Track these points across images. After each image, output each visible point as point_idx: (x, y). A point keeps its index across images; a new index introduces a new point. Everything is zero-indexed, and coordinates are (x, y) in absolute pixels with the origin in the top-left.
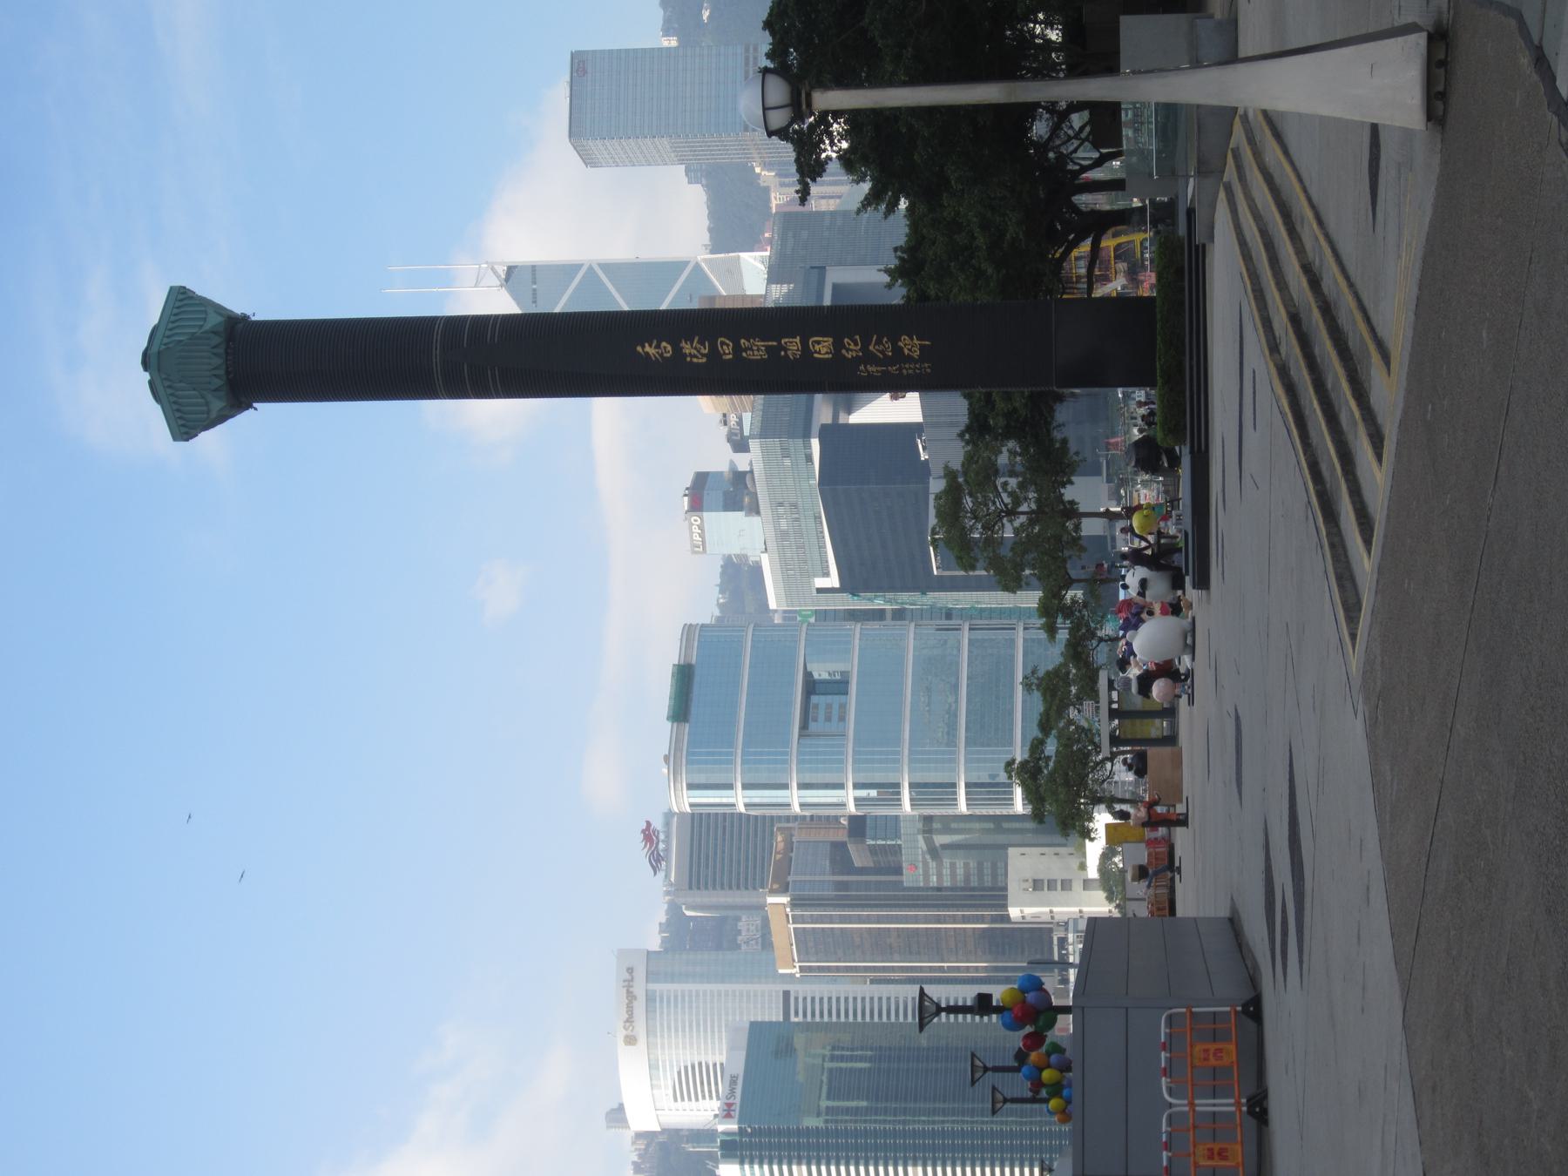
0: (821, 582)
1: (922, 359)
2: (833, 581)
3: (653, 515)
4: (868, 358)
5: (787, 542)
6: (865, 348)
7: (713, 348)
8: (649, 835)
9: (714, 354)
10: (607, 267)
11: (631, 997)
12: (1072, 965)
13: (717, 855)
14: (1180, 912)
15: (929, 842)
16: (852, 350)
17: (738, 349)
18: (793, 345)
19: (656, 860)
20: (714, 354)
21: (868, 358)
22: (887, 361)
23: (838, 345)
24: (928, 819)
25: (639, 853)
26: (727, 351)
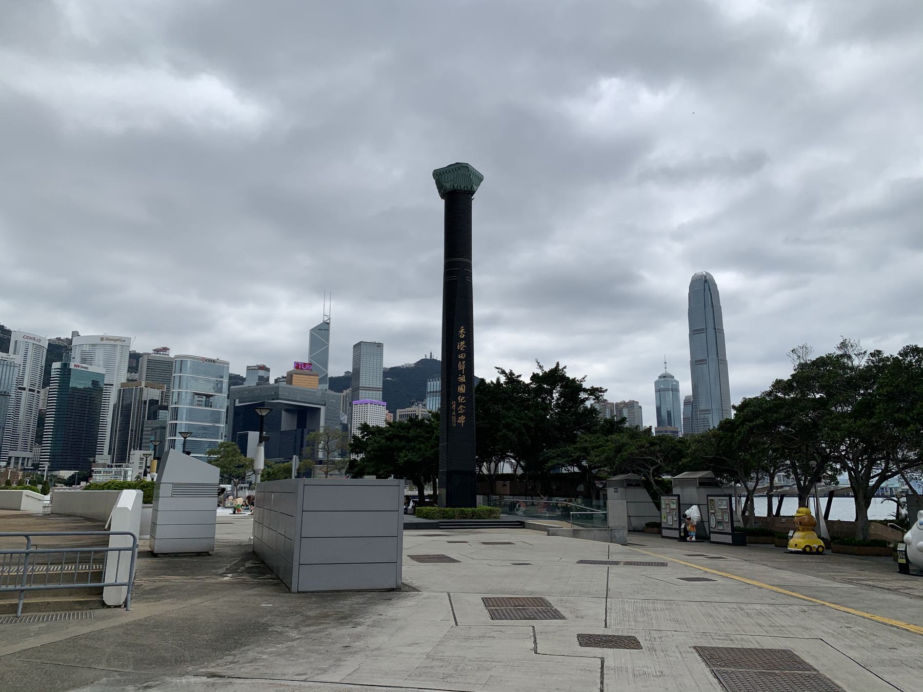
0: (237, 401)
1: (457, 423)
2: (237, 404)
3: (410, 328)
4: (458, 405)
5: (250, 390)
6: (461, 404)
7: (463, 352)
8: (165, 349)
9: (460, 352)
10: (328, 348)
11: (116, 340)
12: (862, 506)
13: (160, 368)
14: (406, 532)
15: (157, 428)
16: (461, 399)
17: (462, 360)
18: (462, 379)
19: (157, 351)
20: (460, 352)
21: (458, 405)
22: (457, 411)
23: (462, 395)
24: (165, 428)
25: (159, 346)
26: (461, 356)
